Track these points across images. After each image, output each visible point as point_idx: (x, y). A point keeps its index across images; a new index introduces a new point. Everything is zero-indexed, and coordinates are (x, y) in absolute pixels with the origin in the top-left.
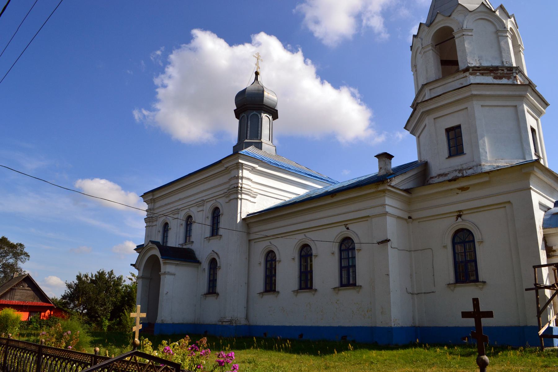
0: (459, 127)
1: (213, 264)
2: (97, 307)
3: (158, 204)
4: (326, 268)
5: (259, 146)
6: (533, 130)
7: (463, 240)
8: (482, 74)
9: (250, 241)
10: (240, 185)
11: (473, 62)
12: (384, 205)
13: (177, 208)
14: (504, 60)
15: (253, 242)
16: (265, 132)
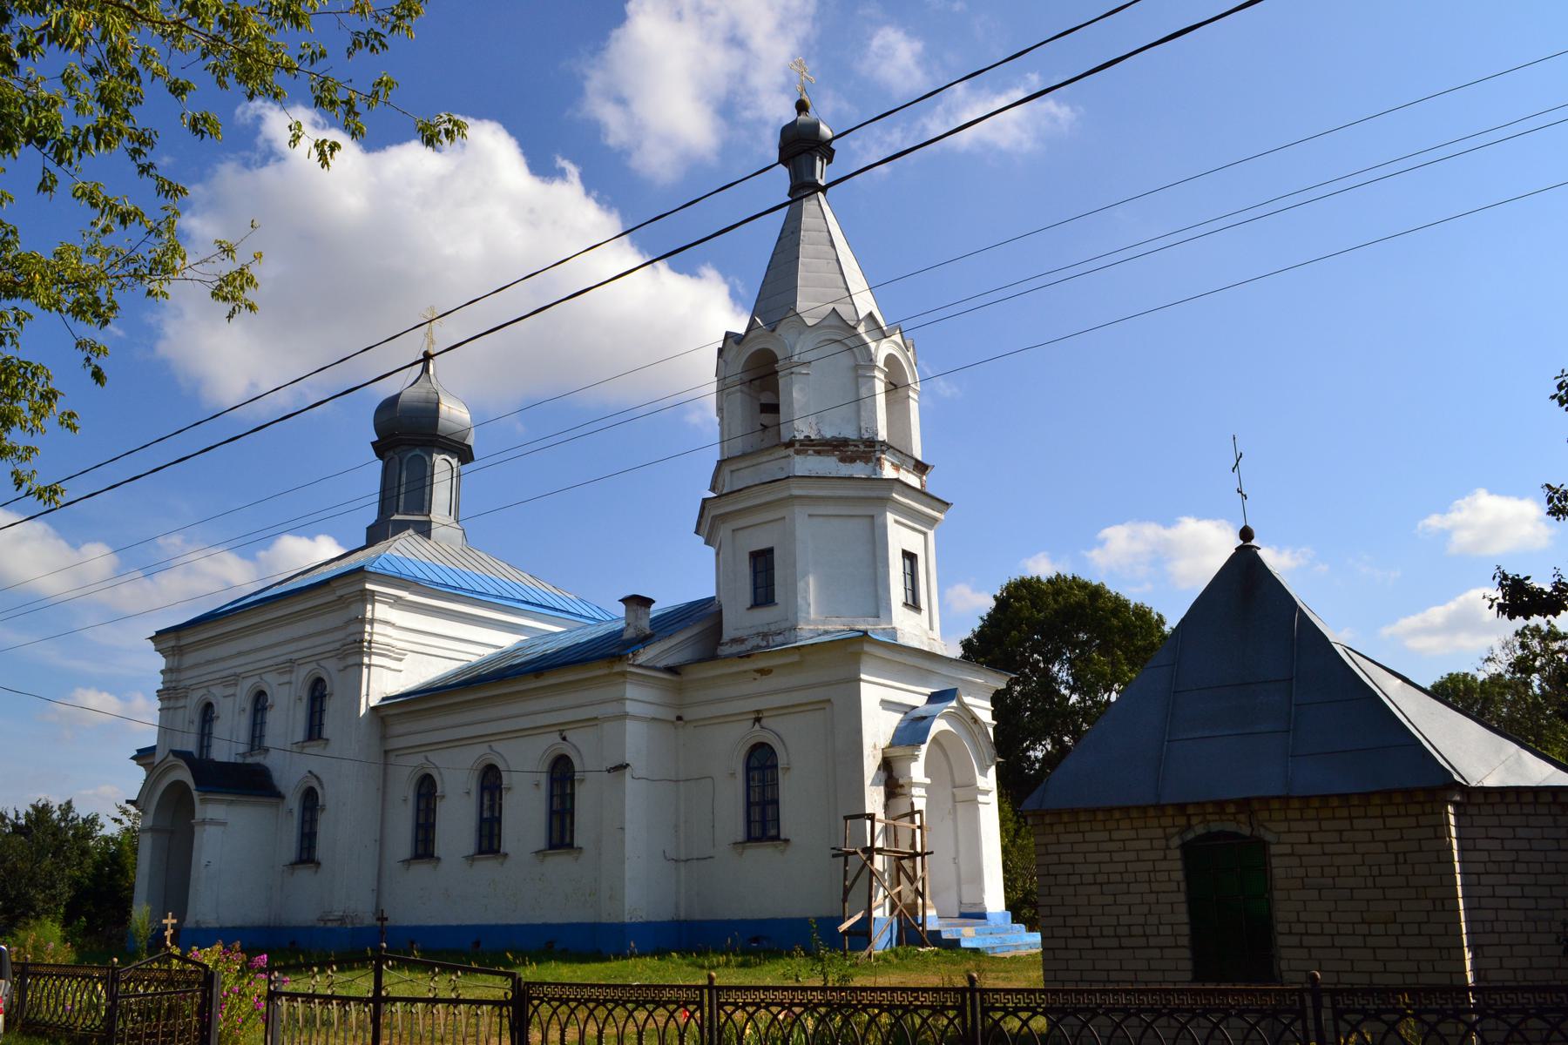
0: (770, 551)
1: (311, 800)
2: (32, 892)
3: (189, 659)
4: (525, 811)
5: (425, 530)
6: (909, 557)
7: (761, 764)
8: (818, 453)
9: (386, 752)
10: (367, 637)
11: (803, 428)
12: (622, 700)
13: (232, 671)
14: (863, 424)
15: (392, 758)
16: (441, 494)
